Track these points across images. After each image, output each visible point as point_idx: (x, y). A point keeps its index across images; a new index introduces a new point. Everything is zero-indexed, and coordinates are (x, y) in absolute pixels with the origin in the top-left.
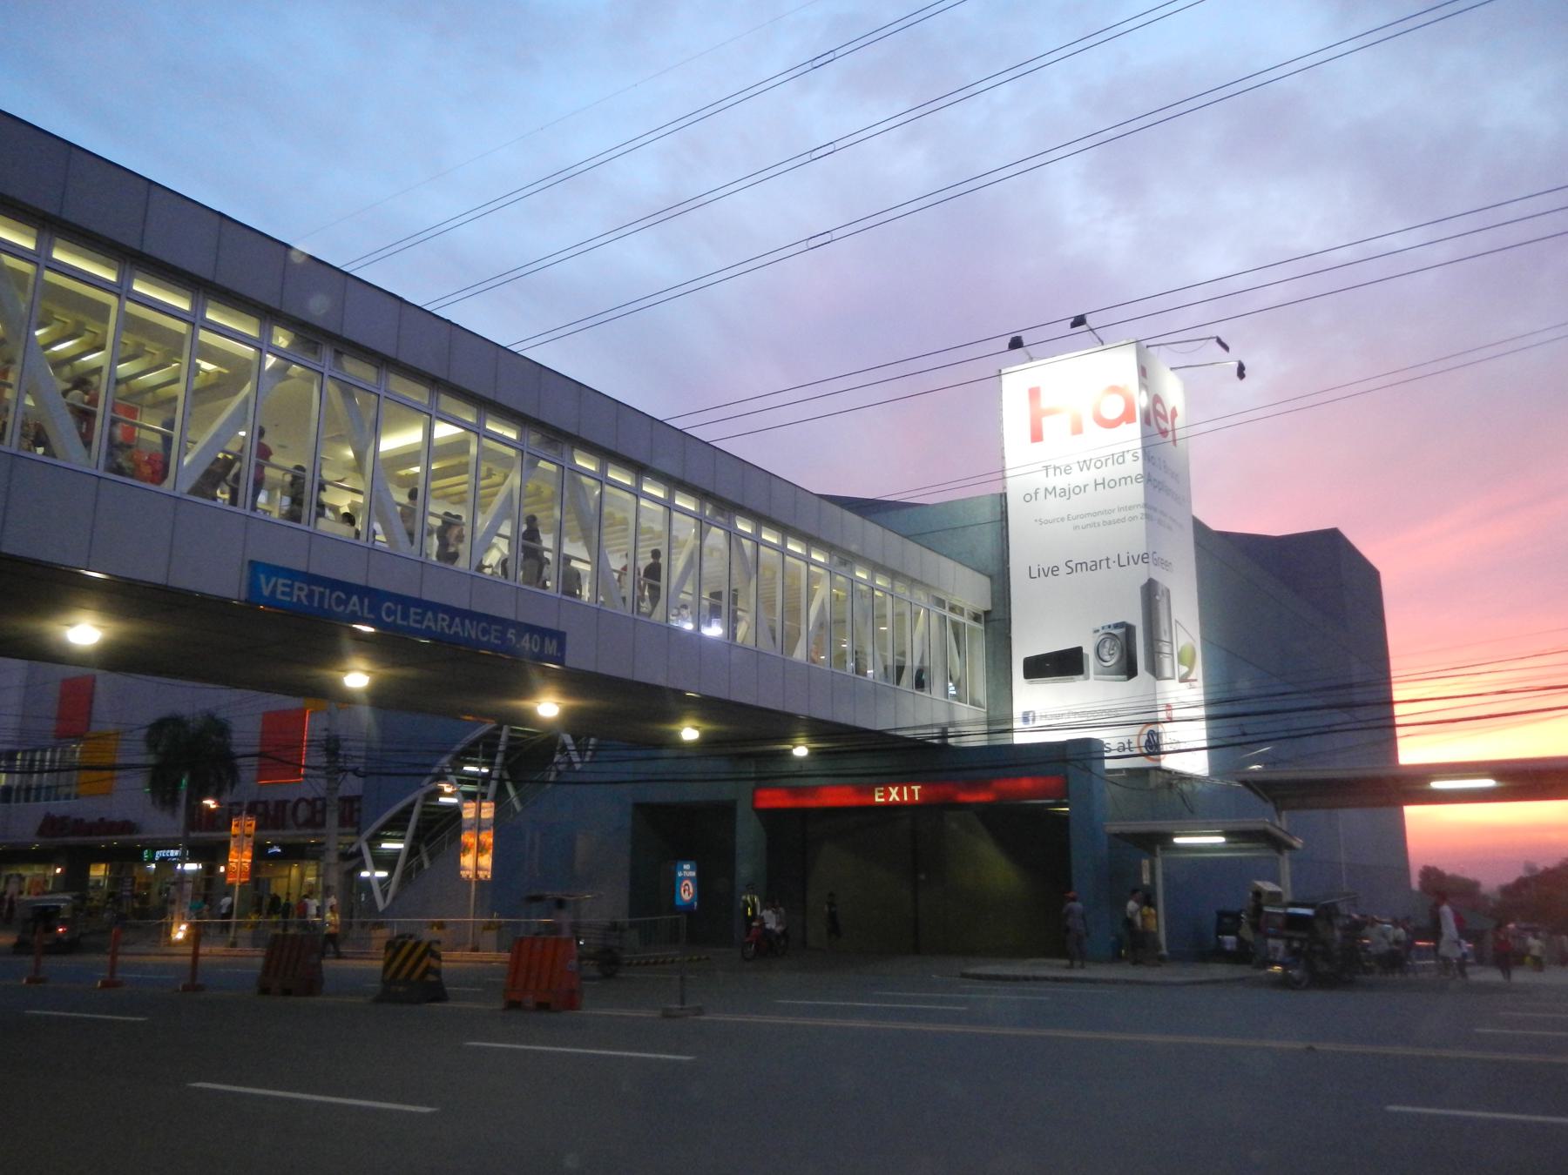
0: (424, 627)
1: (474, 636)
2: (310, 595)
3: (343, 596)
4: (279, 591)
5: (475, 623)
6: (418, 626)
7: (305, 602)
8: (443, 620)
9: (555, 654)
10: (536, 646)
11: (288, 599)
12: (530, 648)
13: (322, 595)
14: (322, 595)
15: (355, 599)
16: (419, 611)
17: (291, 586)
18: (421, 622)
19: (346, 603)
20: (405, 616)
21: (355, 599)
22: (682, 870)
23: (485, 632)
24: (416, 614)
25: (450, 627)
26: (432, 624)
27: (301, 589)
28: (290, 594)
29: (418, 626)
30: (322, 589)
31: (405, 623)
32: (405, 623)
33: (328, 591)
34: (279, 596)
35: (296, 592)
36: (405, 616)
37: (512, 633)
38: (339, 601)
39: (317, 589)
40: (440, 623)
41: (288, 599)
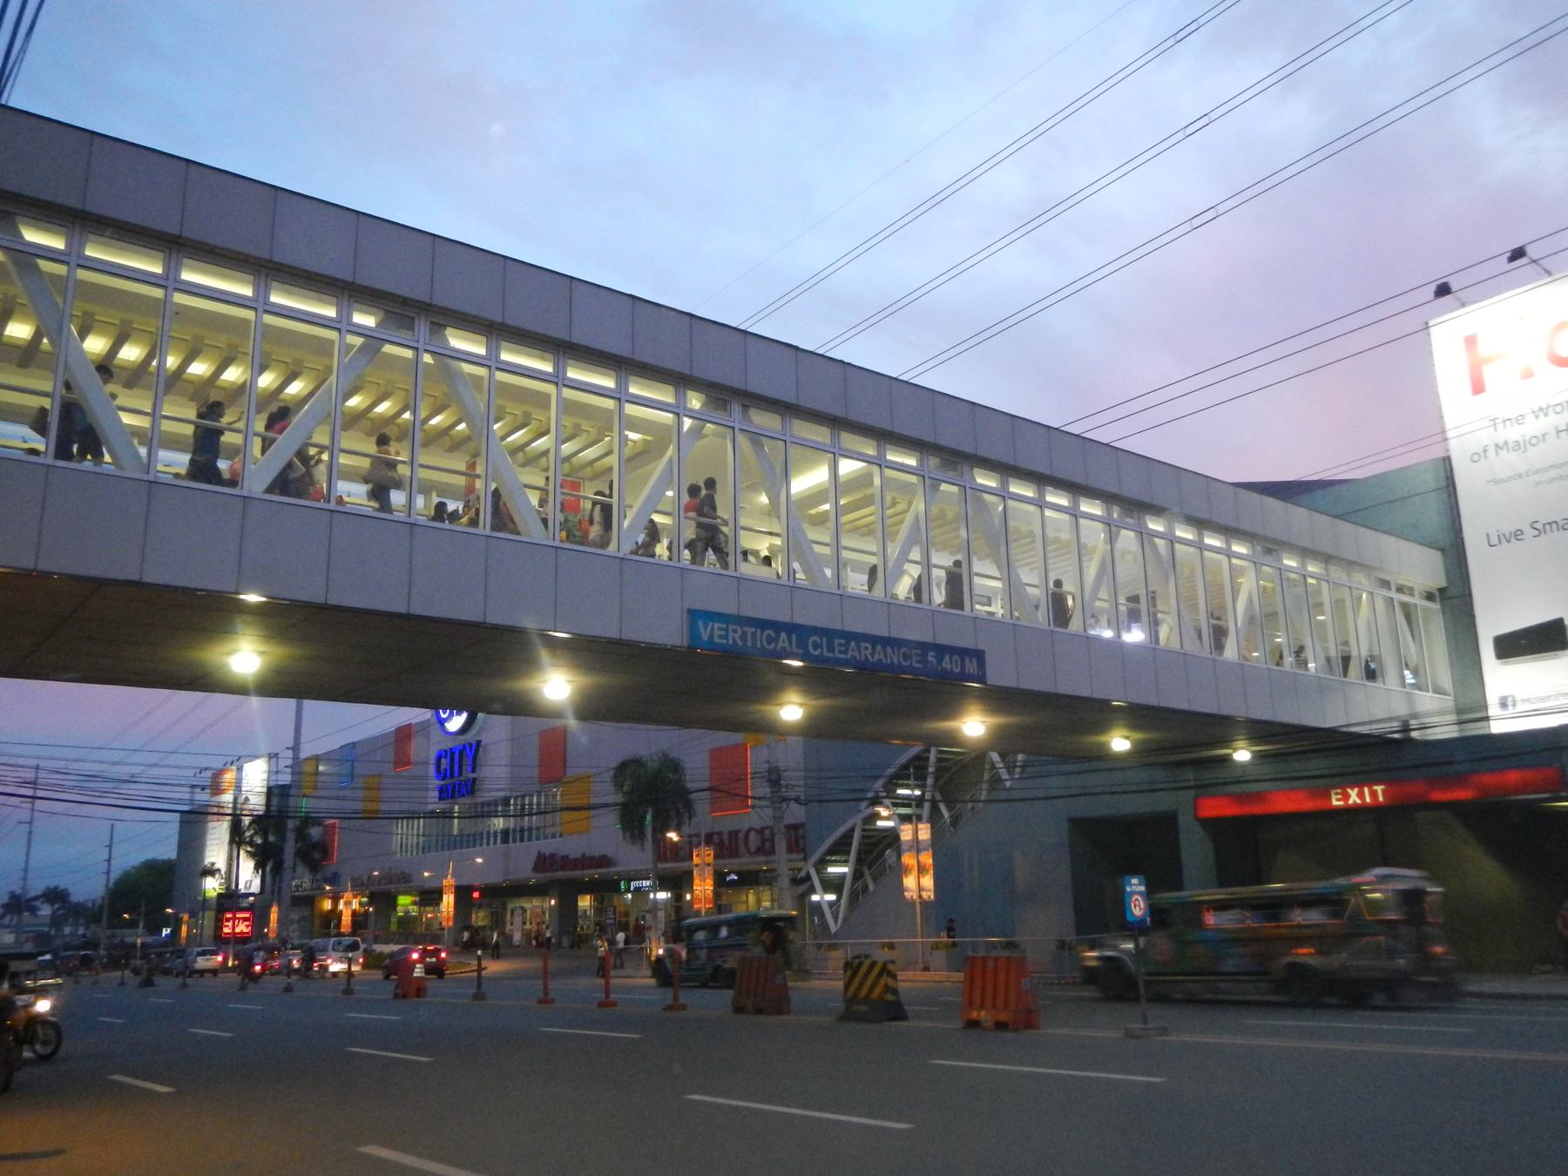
0: (849, 656)
1: (896, 662)
2: (744, 636)
3: (773, 635)
4: (716, 636)
5: (896, 648)
6: (843, 656)
7: (740, 644)
8: (866, 648)
9: (976, 673)
10: (957, 667)
11: (725, 641)
12: (952, 668)
13: (754, 634)
14: (754, 634)
15: (783, 635)
16: (843, 641)
17: (726, 630)
18: (845, 652)
19: (776, 640)
20: (831, 649)
21: (783, 635)
22: (1131, 885)
23: (906, 657)
24: (840, 645)
25: (873, 654)
26: (856, 654)
27: (735, 631)
28: (726, 637)
29: (843, 656)
30: (753, 630)
31: (831, 655)
32: (831, 655)
33: (759, 631)
34: (717, 640)
35: (731, 634)
36: (831, 649)
37: (933, 656)
38: (770, 640)
39: (750, 630)
40: (863, 652)
41: (725, 641)
